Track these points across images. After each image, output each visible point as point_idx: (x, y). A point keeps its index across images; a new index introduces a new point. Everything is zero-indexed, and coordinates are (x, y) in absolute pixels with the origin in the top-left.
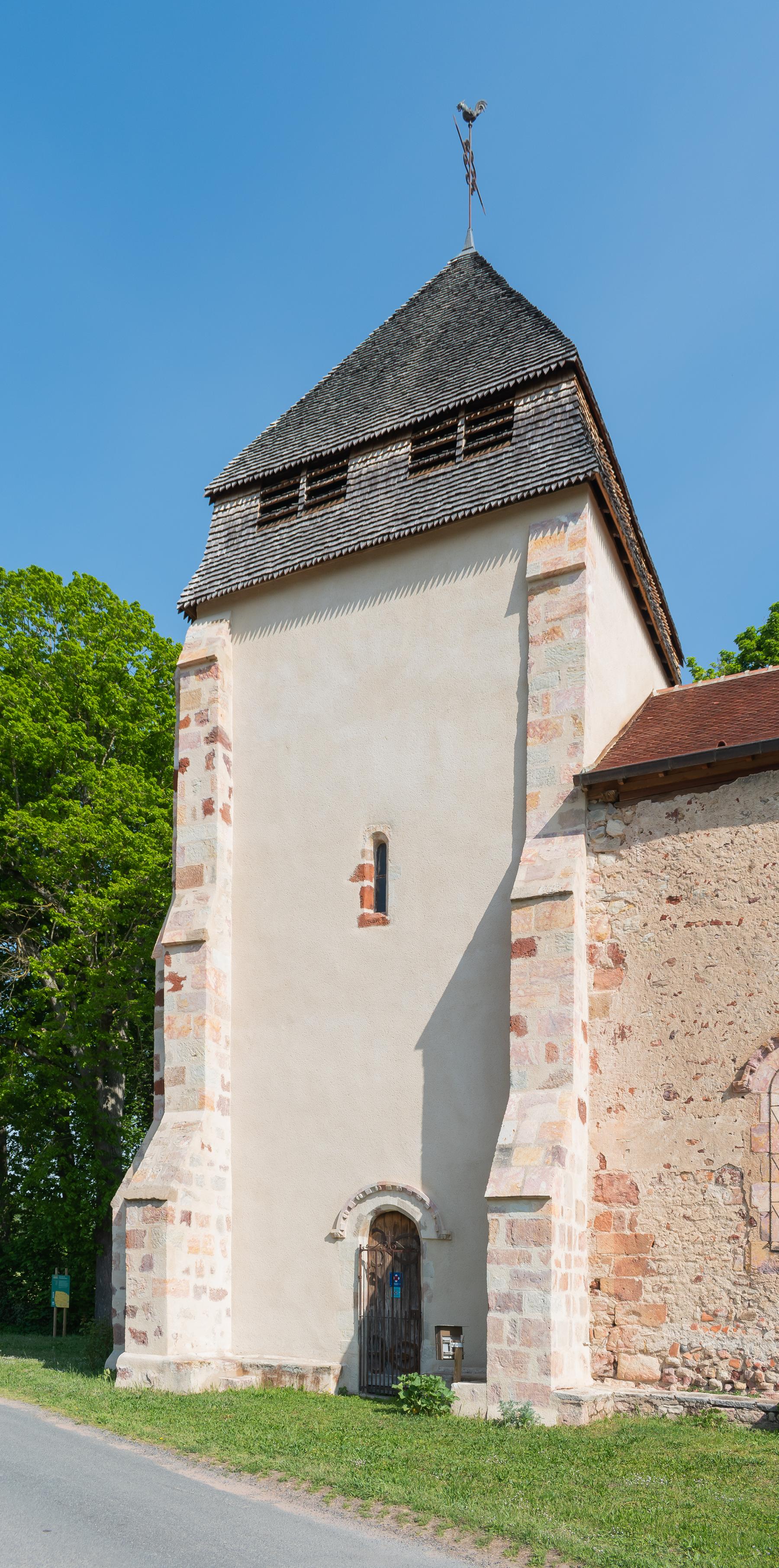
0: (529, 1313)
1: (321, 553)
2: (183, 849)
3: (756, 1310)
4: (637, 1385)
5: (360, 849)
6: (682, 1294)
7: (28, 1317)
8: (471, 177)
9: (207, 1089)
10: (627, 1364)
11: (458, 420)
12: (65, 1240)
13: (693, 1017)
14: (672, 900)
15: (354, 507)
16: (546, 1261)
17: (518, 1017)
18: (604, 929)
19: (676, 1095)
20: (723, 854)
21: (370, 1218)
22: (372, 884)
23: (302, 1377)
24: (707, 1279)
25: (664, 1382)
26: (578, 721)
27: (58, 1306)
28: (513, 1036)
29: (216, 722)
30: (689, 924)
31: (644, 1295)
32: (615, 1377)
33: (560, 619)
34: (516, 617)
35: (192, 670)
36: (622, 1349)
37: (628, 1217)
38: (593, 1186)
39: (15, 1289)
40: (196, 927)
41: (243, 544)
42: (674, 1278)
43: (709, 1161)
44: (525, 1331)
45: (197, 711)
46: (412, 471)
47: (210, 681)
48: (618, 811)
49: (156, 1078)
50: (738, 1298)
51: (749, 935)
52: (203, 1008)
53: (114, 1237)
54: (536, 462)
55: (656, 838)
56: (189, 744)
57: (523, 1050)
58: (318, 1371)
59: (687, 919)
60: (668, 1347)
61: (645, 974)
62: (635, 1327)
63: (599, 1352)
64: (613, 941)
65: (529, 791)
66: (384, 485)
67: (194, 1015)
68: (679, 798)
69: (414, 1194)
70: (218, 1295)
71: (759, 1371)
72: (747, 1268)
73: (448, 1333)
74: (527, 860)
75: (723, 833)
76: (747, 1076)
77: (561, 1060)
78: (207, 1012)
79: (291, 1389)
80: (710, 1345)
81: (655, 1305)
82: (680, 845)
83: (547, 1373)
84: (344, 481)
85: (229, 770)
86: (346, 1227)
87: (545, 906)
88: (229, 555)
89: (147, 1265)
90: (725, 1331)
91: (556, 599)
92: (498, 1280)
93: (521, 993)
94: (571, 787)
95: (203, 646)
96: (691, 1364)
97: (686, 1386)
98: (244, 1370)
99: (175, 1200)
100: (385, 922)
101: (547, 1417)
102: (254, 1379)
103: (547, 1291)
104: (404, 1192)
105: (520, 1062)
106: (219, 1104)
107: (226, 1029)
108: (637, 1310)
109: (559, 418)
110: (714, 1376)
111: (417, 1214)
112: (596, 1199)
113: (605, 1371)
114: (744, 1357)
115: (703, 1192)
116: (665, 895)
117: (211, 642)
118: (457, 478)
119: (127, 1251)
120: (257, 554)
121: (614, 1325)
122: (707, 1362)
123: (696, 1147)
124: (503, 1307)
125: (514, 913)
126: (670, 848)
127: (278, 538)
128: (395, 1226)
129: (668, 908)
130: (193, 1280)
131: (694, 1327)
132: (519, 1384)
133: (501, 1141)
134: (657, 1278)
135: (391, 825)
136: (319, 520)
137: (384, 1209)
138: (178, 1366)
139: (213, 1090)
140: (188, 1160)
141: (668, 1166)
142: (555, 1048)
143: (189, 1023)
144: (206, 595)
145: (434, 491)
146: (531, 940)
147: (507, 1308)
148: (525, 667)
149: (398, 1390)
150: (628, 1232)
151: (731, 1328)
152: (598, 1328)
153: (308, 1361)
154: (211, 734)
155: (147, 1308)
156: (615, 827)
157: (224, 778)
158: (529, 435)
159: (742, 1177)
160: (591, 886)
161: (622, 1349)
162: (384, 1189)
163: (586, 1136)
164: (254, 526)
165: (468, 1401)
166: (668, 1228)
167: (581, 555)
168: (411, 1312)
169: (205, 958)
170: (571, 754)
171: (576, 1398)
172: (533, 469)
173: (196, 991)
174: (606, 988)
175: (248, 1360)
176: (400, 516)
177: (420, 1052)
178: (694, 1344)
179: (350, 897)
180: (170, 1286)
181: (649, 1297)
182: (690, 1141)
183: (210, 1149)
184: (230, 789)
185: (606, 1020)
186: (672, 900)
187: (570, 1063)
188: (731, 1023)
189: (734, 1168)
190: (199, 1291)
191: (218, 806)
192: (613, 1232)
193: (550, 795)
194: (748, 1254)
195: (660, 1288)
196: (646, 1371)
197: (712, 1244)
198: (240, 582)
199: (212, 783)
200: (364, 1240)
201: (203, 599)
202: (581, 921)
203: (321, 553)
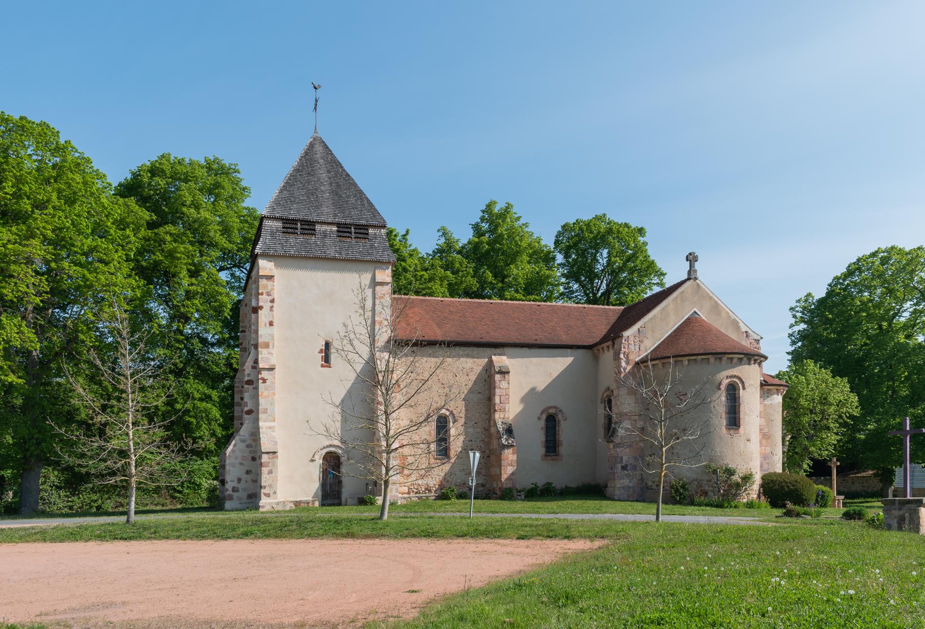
8: (315, 108)
25: (409, 493)
56: (263, 301)
89: (270, 472)
111: (340, 451)
117: (271, 270)
155: (270, 486)
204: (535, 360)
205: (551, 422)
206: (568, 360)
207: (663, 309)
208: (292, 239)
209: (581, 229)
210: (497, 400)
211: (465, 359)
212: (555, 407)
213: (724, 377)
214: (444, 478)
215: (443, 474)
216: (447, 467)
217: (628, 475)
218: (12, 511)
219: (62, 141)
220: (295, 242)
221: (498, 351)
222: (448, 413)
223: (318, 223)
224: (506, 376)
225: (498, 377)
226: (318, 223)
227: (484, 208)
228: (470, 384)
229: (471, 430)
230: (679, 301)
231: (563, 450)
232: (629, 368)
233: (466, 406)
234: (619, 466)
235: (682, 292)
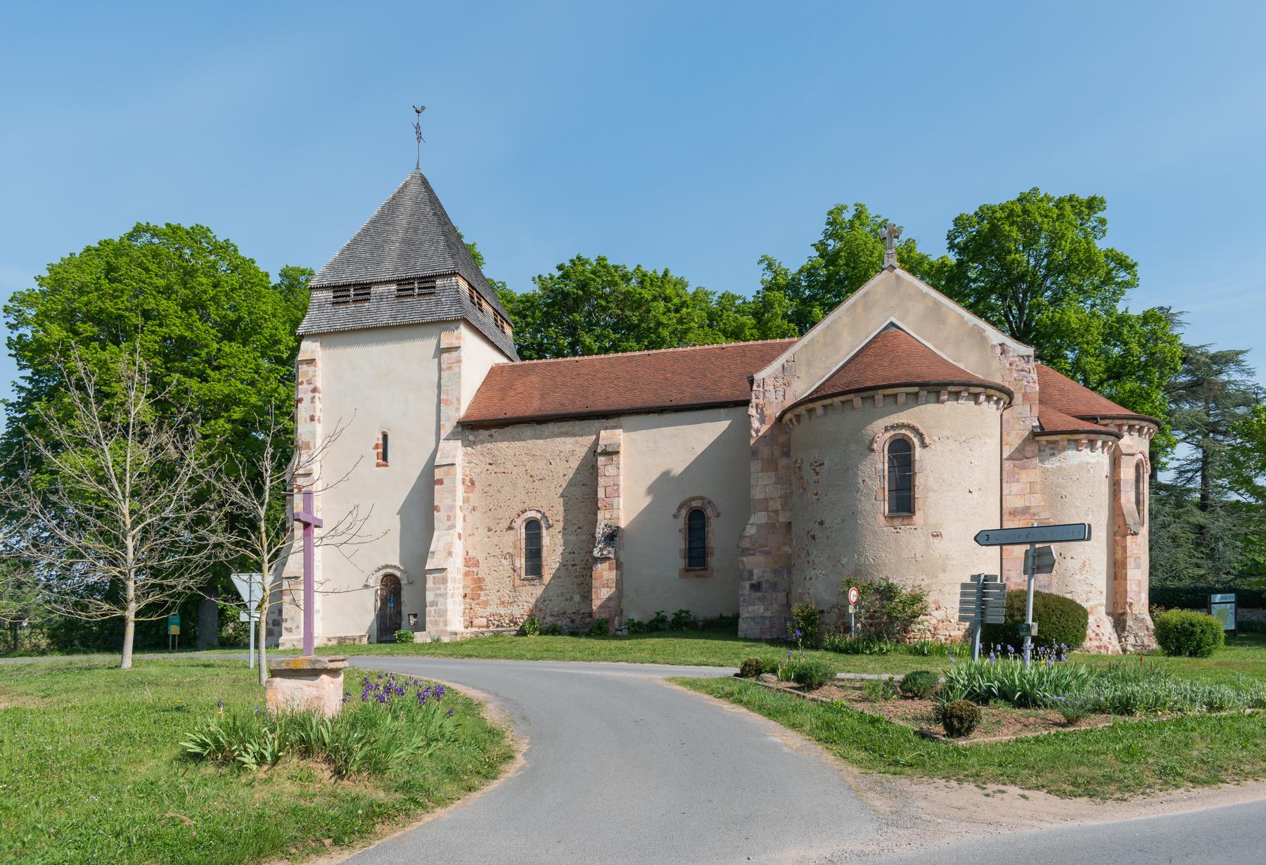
0: (440, 606)
10: (476, 622)
26: (458, 400)
56: (303, 391)
75: (506, 444)
80: (502, 612)
101: (446, 639)
102: (334, 642)
111: (398, 574)
117: (313, 352)
133: (432, 549)
148: (440, 378)
153: (357, 633)
155: (292, 619)
156: (471, 438)
157: (318, 405)
162: (387, 566)
179: (373, 456)
181: (483, 598)
193: (447, 428)
198: (325, 329)
202: (459, 472)
204: (666, 431)
205: (696, 521)
206: (723, 425)
207: (828, 327)
208: (342, 310)
209: (992, 221)
210: (601, 494)
211: (562, 439)
212: (701, 498)
213: (881, 430)
214: (536, 606)
215: (533, 601)
216: (539, 591)
217: (762, 599)
218: (6, 654)
220: (345, 315)
221: (611, 422)
222: (539, 516)
223: (376, 283)
225: (601, 460)
226: (376, 283)
227: (174, 223)
228: (571, 474)
230: (859, 309)
231: (713, 561)
232: (764, 429)
233: (565, 504)
234: (747, 584)
235: (866, 294)
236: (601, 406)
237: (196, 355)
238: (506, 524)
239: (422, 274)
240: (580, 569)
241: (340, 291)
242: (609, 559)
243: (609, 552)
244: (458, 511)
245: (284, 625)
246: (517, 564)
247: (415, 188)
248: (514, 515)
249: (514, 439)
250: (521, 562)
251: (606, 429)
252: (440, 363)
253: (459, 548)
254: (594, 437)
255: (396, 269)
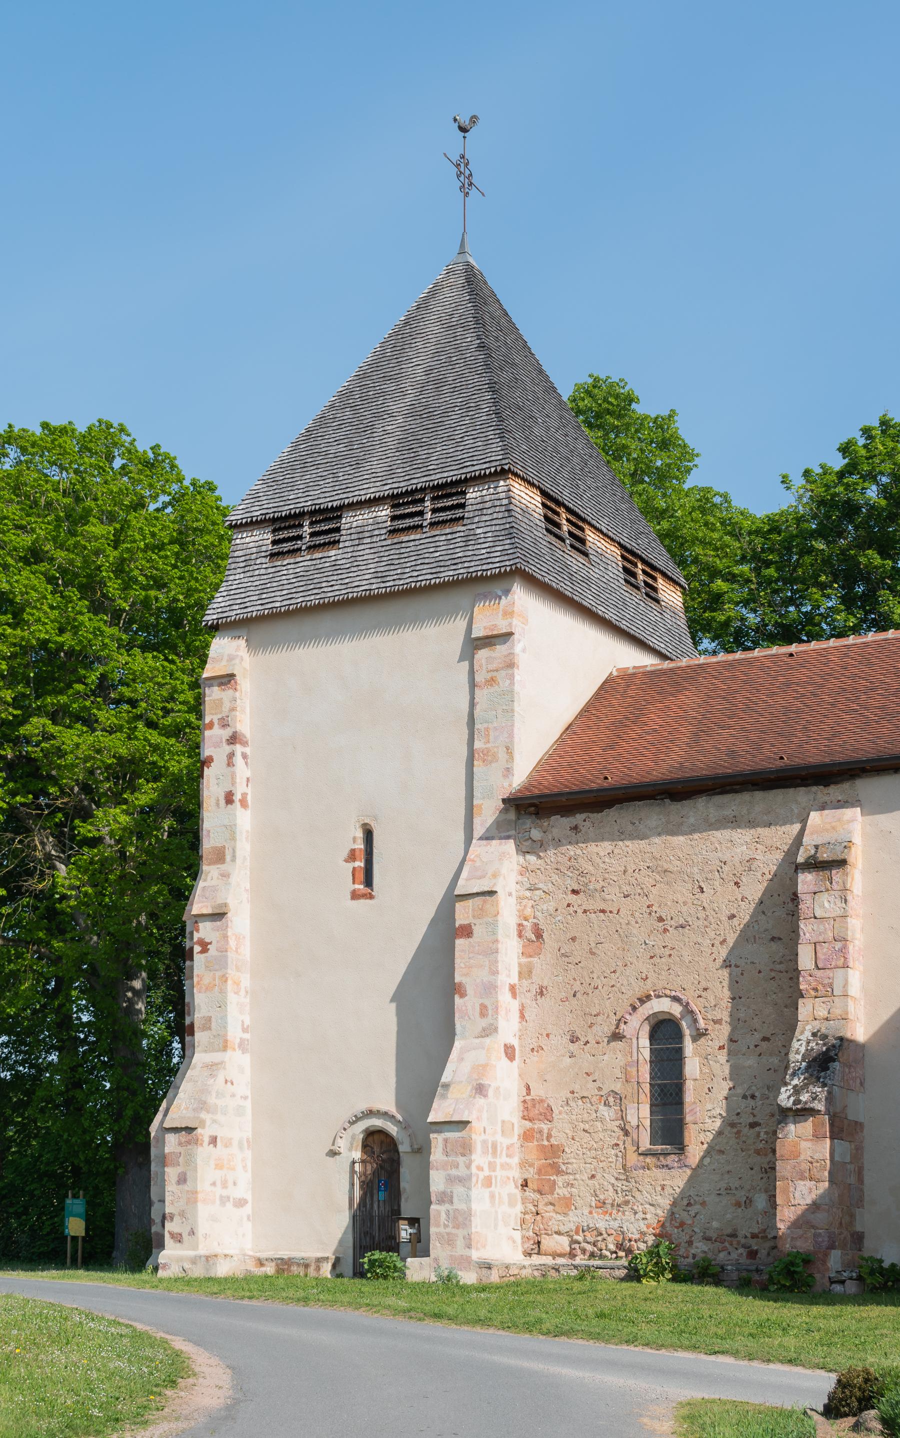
0: (458, 1205)
1: (318, 597)
2: (209, 831)
3: (630, 1198)
4: (554, 1259)
5: (352, 836)
6: (582, 1188)
7: (35, 1250)
9: (229, 1034)
10: (548, 1243)
11: (426, 495)
12: (82, 1158)
13: (588, 980)
14: (574, 892)
15: (345, 556)
16: (468, 1167)
17: (460, 984)
18: (529, 911)
19: (578, 1039)
20: (607, 860)
21: (361, 1136)
22: (362, 865)
23: (307, 1266)
24: (598, 1176)
25: (572, 1255)
26: (509, 751)
27: (72, 1234)
28: (457, 997)
29: (235, 727)
30: (585, 911)
31: (557, 1190)
32: (539, 1253)
33: (497, 671)
34: (466, 664)
35: (215, 682)
36: (543, 1232)
37: (546, 1131)
38: (522, 1108)
39: (19, 1218)
40: (220, 901)
41: (257, 572)
42: (577, 1176)
43: (600, 1089)
44: (455, 1218)
45: (220, 716)
46: (393, 532)
47: (230, 692)
48: (538, 821)
49: (187, 1021)
50: (619, 1189)
51: (624, 921)
52: (226, 968)
53: (152, 1157)
54: (479, 546)
55: (563, 845)
56: (213, 743)
57: (464, 1008)
58: (319, 1260)
59: (584, 907)
60: (574, 1228)
61: (557, 947)
62: (551, 1214)
63: (527, 1235)
64: (535, 921)
65: (475, 803)
66: (368, 540)
67: (218, 974)
68: (578, 816)
69: (393, 1117)
70: (240, 1203)
71: (632, 1243)
72: (624, 1167)
73: (406, 1222)
74: (470, 860)
75: (607, 846)
76: (622, 1026)
77: (490, 1016)
78: (229, 971)
79: (298, 1276)
80: (601, 1225)
81: (565, 1198)
82: (579, 852)
83: (469, 1247)
84: (338, 530)
85: (246, 763)
86: (342, 1145)
87: (478, 900)
88: (246, 580)
89: (182, 1180)
90: (611, 1214)
91: (493, 655)
92: (437, 1181)
93: (462, 965)
94: (502, 806)
95: (224, 663)
96: (589, 1240)
97: (586, 1257)
98: (261, 1263)
99: (204, 1127)
100: (371, 897)
101: (469, 1278)
102: (270, 1269)
103: (469, 1189)
104: (385, 1115)
105: (462, 1018)
106: (240, 1045)
107: (246, 981)
108: (553, 1201)
109: (497, 509)
110: (604, 1248)
112: (524, 1118)
113: (532, 1249)
114: (623, 1233)
115: (596, 1112)
116: (570, 889)
117: (231, 658)
118: (423, 547)
119: (166, 1169)
120: (269, 585)
121: (538, 1214)
122: (600, 1238)
123: (591, 1078)
124: (441, 1202)
125: (457, 905)
126: (572, 853)
127: (285, 572)
128: (382, 1142)
129: (572, 898)
130: (219, 1191)
131: (591, 1213)
132: (451, 1256)
133: (444, 1079)
134: (566, 1177)
135: (375, 818)
136: (318, 562)
137: (371, 1129)
138: (207, 1258)
139: (234, 1033)
140: (214, 1095)
141: (572, 1092)
142: (486, 1007)
143: (214, 980)
144: (227, 617)
145: (406, 555)
146: (470, 925)
147: (443, 1201)
148: (472, 705)
149: (364, 1263)
150: (546, 1143)
151: (615, 1212)
152: (526, 1216)
153: (311, 1252)
154: (231, 737)
155: (182, 1214)
156: (536, 834)
157: (242, 770)
158: (476, 519)
159: (621, 1100)
160: (520, 877)
161: (543, 1232)
162: (370, 1113)
163: (517, 1070)
164: (266, 557)
165: (417, 1270)
166: (573, 1139)
167: (510, 625)
168: (392, 1210)
169: (227, 926)
170: (505, 776)
171: (488, 1264)
172: (476, 552)
173: (220, 954)
174: (531, 956)
175: (263, 1255)
176: (380, 575)
177: (394, 1005)
178: (591, 1226)
179: (344, 874)
180: (200, 1196)
181: (561, 1191)
182: (587, 1073)
183: (232, 1084)
184: (248, 779)
185: (530, 981)
186: (574, 892)
187: (496, 1019)
188: (613, 986)
189: (616, 1093)
190: (224, 1200)
191: (237, 797)
192: (536, 1143)
193: (489, 811)
194: (624, 1157)
195: (568, 1184)
196: (559, 1248)
197: (602, 1150)
198: (254, 610)
199: (232, 778)
200: (357, 1155)
201: (224, 620)
202: (508, 911)
203: (318, 597)
208: (292, 568)
210: (805, 960)
216: (678, 1180)
218: (46, 1251)
219: (838, 463)
221: (835, 792)
222: (676, 1010)
223: (352, 506)
224: (837, 875)
226: (352, 506)
228: (745, 913)
229: (751, 1062)
233: (734, 983)
236: (814, 752)
237: (81, 680)
238: (608, 1028)
239: (438, 478)
240: (755, 1129)
241: (283, 525)
242: (812, 1112)
243: (815, 1096)
244: (505, 997)
245: (169, 1226)
246: (632, 1120)
247: (454, 296)
248: (623, 1008)
249: (622, 835)
250: (641, 1113)
251: (823, 808)
252: (472, 666)
253: (507, 1079)
254: (797, 827)
255: (391, 472)
